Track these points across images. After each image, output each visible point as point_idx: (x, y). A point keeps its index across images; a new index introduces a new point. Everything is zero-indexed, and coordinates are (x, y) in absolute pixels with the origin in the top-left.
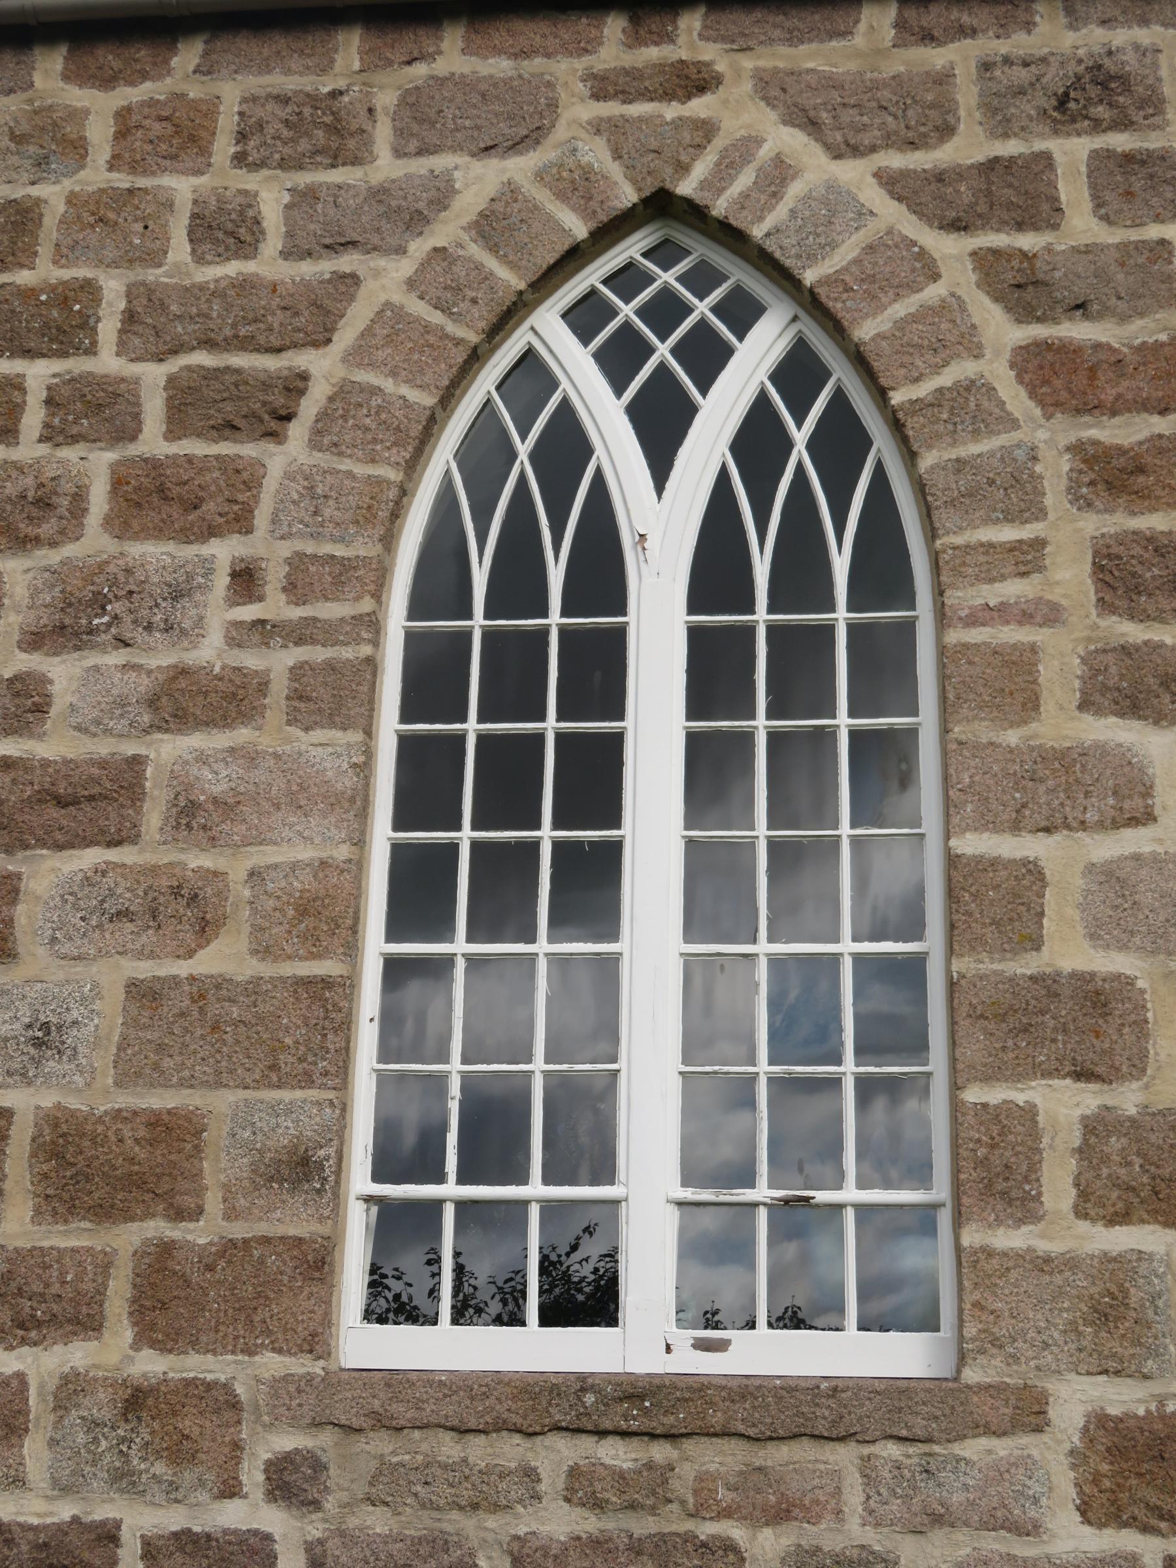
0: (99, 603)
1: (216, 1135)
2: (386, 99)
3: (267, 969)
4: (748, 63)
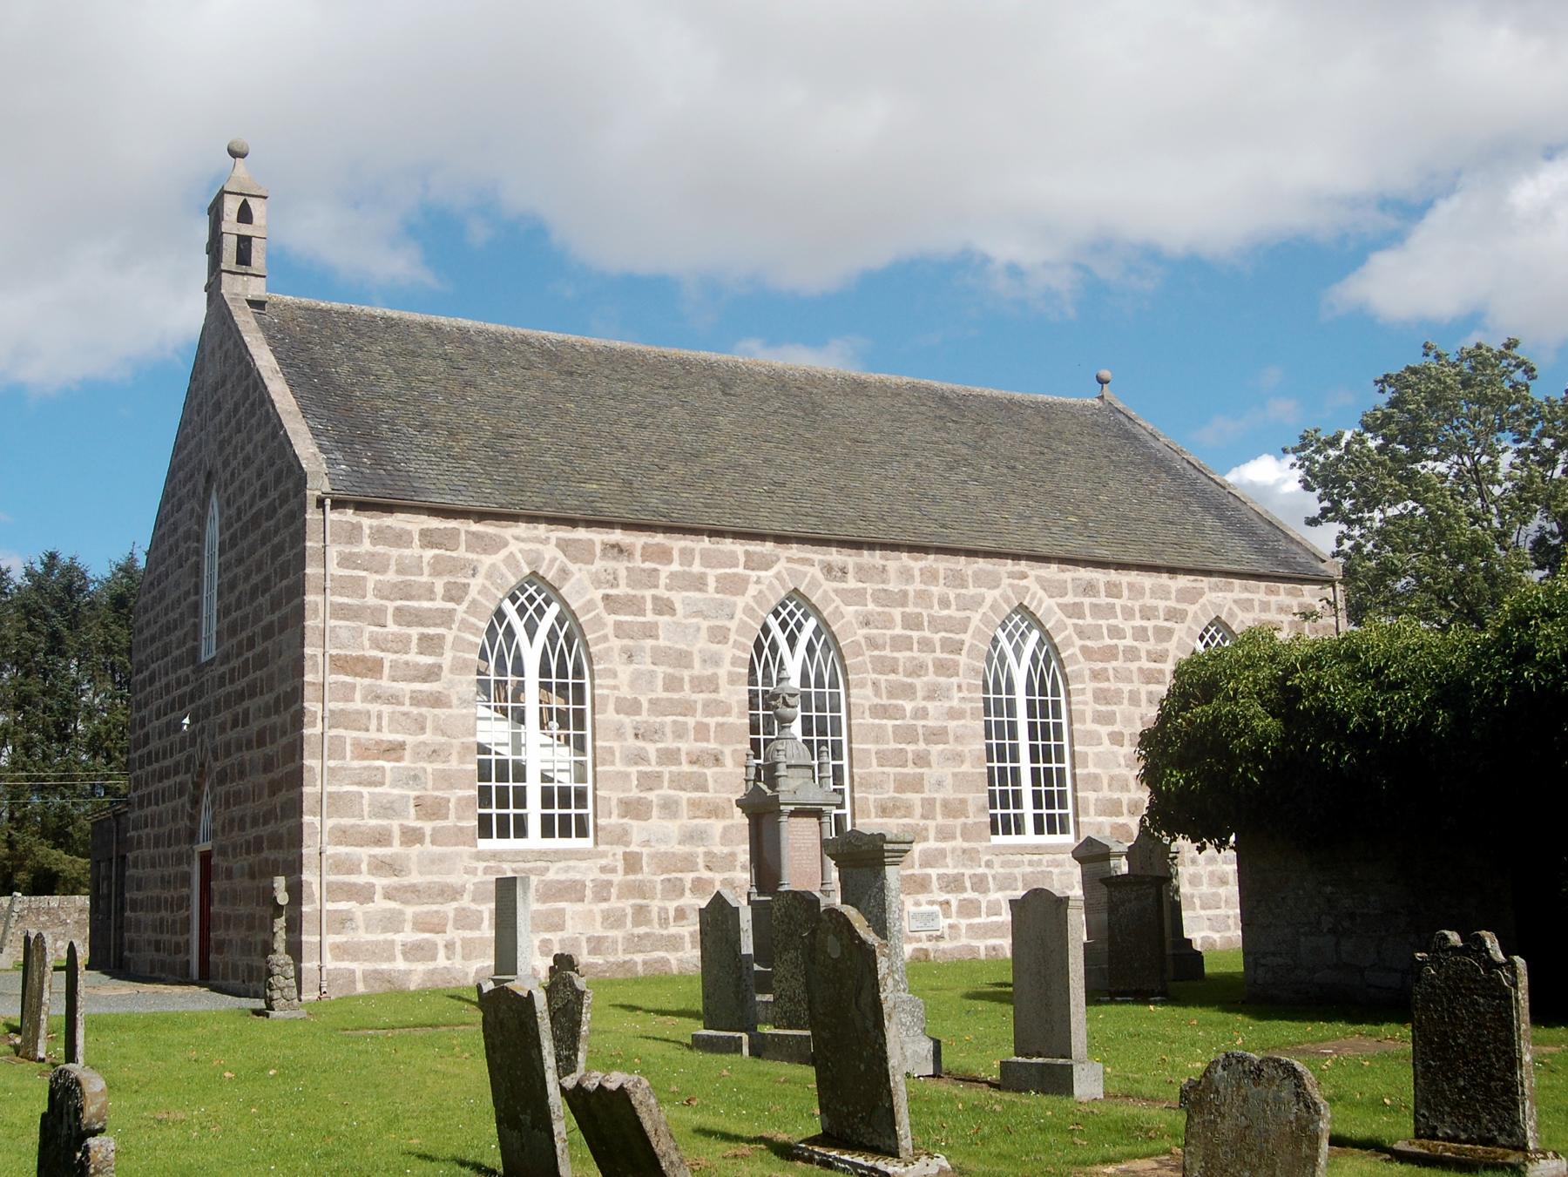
0: (935, 691)
1: (970, 802)
2: (970, 572)
3: (974, 770)
4: (1033, 573)
